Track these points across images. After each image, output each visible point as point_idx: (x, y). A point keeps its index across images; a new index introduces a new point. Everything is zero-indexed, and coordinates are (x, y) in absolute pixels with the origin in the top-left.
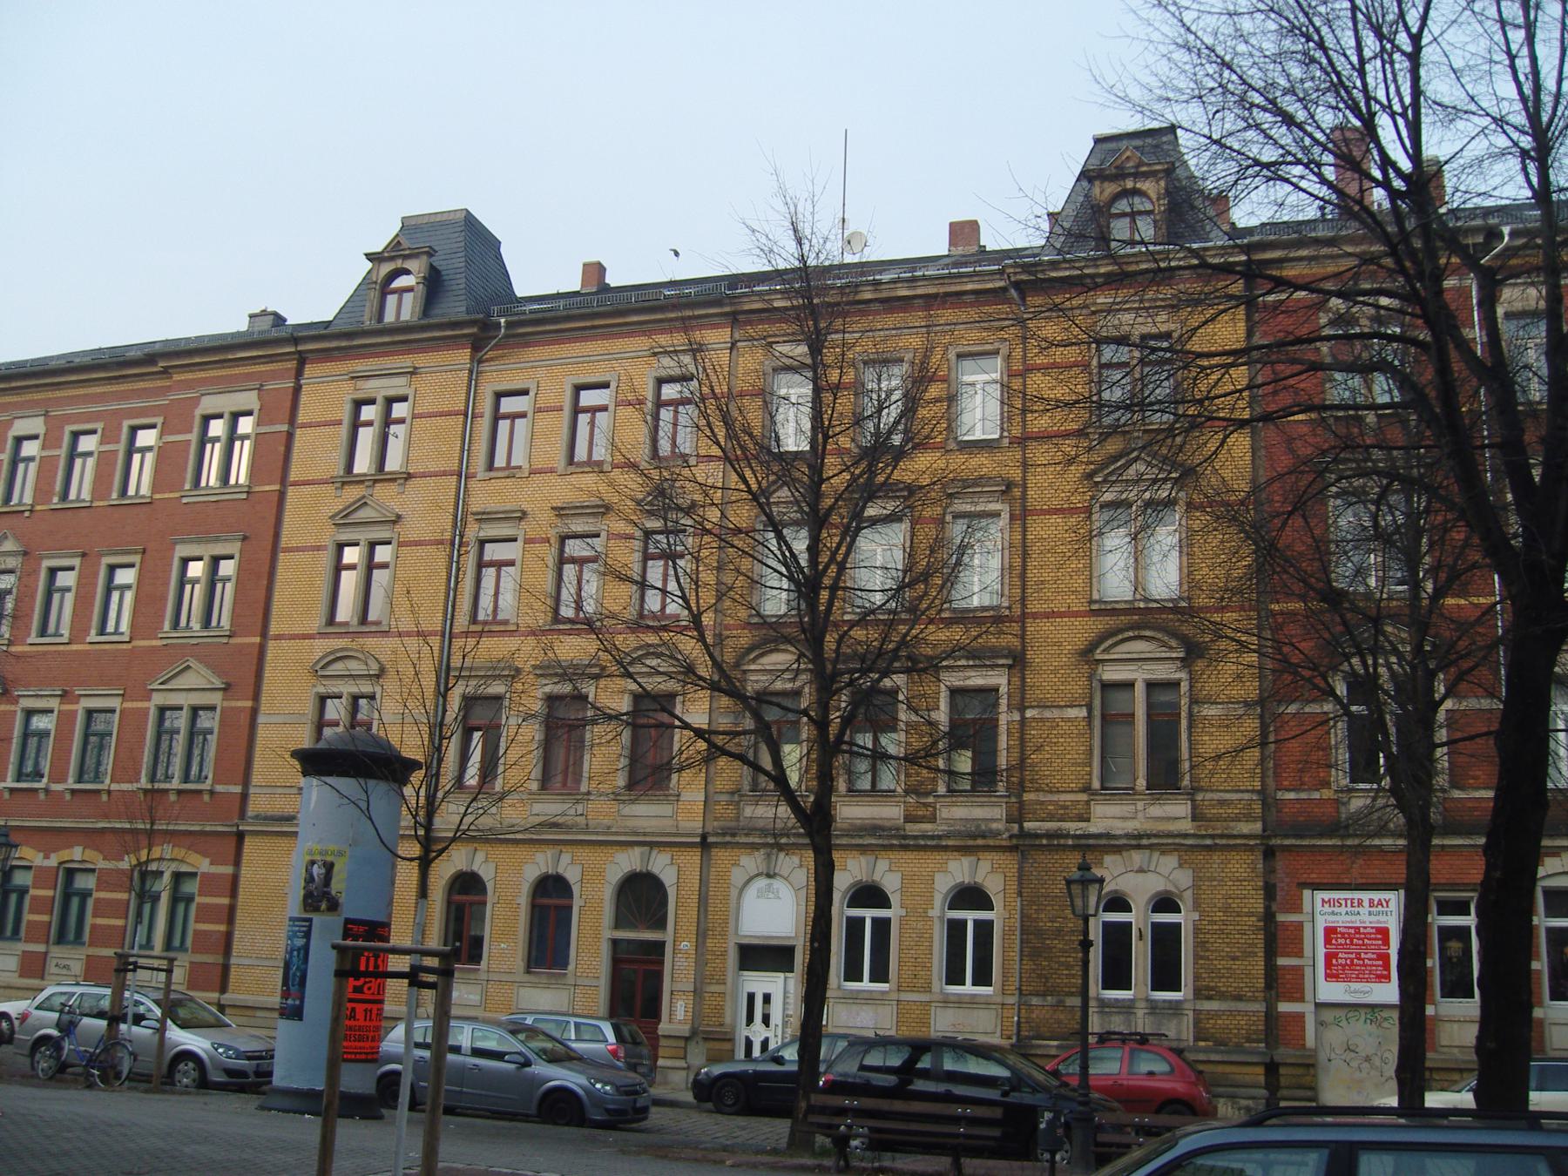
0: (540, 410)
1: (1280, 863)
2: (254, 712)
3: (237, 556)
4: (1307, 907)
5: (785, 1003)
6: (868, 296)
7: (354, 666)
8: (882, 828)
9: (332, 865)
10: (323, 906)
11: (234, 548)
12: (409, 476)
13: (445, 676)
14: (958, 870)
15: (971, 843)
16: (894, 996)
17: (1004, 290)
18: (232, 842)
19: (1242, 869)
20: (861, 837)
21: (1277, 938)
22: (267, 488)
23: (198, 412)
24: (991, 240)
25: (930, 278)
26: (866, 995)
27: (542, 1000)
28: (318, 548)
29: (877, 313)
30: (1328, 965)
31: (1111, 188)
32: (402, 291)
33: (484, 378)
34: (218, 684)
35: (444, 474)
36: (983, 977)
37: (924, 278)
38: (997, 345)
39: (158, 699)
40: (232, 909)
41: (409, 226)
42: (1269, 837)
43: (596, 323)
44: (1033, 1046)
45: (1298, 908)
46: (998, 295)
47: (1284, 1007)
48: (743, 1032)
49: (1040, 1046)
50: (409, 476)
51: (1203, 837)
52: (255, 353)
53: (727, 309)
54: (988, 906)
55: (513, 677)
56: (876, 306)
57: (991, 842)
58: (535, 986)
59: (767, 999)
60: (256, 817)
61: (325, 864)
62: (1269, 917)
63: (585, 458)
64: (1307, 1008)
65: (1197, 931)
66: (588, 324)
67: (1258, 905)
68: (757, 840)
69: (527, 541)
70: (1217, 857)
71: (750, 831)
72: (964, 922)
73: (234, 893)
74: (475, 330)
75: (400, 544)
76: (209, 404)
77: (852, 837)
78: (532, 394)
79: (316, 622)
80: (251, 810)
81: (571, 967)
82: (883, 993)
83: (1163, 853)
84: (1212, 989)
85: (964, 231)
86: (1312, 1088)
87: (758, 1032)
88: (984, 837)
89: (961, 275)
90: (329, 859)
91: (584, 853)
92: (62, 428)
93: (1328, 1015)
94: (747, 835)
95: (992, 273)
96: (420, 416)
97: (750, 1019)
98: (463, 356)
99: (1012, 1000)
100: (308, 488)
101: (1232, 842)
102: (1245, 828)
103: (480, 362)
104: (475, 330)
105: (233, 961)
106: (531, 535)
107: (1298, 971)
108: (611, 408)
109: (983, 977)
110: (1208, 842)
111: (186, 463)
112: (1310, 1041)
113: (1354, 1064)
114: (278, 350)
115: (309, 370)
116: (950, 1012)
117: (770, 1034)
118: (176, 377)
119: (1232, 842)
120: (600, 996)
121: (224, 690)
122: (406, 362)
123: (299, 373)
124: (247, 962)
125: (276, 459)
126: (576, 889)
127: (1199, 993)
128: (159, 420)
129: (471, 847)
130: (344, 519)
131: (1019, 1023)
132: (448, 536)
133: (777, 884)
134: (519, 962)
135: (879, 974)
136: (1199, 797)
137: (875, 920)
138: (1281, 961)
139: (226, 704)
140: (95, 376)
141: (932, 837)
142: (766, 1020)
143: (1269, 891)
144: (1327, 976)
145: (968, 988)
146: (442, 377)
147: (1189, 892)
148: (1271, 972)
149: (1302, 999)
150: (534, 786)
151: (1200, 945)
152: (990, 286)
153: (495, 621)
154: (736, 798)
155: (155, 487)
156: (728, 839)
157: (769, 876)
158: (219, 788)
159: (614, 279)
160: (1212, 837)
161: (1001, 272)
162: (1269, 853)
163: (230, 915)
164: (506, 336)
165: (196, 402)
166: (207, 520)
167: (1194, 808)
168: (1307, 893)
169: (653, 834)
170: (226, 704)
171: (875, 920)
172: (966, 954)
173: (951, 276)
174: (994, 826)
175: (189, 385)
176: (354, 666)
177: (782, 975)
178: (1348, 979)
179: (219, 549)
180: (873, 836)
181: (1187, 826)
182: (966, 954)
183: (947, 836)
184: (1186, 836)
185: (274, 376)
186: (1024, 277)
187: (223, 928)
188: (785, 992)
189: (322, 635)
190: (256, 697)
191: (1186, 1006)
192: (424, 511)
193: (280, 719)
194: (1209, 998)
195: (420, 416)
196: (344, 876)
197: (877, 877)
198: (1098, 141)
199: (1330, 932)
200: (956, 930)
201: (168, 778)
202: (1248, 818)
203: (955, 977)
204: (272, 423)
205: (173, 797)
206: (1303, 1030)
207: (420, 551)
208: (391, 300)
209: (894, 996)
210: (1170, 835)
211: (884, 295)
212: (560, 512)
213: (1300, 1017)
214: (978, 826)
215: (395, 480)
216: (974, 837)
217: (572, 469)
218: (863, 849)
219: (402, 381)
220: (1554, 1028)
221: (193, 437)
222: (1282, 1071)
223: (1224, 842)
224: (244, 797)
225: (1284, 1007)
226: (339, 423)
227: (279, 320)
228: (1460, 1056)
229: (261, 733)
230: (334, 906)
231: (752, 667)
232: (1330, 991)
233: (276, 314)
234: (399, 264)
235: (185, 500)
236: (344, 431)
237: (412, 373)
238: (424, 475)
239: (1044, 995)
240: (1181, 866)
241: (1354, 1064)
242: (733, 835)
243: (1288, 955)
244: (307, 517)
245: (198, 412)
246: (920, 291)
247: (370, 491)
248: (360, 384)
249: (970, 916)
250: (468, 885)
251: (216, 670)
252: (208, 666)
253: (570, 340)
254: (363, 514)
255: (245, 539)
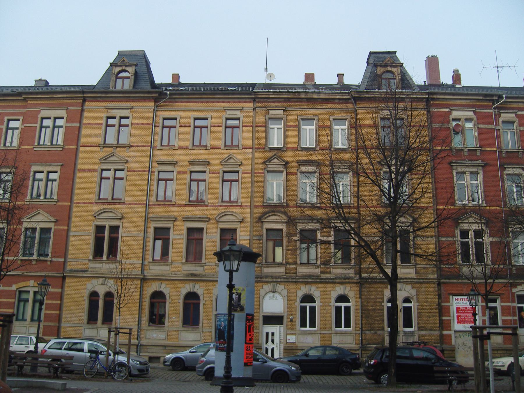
0: (181, 126)
1: (443, 287)
2: (68, 231)
3: (59, 172)
4: (451, 301)
5: (280, 335)
6: (303, 97)
7: (110, 215)
8: (313, 276)
9: (241, 294)
10: (238, 309)
11: (58, 169)
12: (131, 146)
13: (147, 219)
14: (339, 290)
15: (344, 281)
16: (319, 332)
17: (349, 99)
18: (60, 280)
19: (431, 290)
20: (306, 279)
21: (443, 311)
22: (71, 147)
23: (40, 116)
24: (318, 80)
25: (325, 93)
26: (309, 332)
27: (189, 336)
28: (94, 171)
29: (304, 102)
30: (458, 319)
31: (383, 69)
32: (124, 78)
33: (158, 113)
34: (53, 219)
35: (145, 146)
36: (347, 325)
37: (323, 92)
38: (346, 117)
39: (25, 225)
40: (61, 305)
41: (121, 54)
42: (440, 279)
43: (241, 96)
44: (368, 347)
45: (448, 301)
46: (346, 101)
47: (445, 332)
48: (265, 346)
49: (370, 347)
50: (131, 146)
51: (420, 279)
52: (65, 96)
53: (253, 96)
54: (349, 302)
55: (174, 221)
56: (305, 100)
57: (351, 281)
58: (186, 331)
59: (273, 334)
60: (71, 270)
61: (238, 294)
62: (439, 304)
63: (198, 144)
64: (452, 332)
65: (418, 309)
66: (201, 97)
67: (436, 300)
68: (270, 280)
69: (128, 171)
70: (423, 286)
71: (267, 277)
72: (306, 307)
73: (61, 299)
74: (157, 95)
75: (128, 171)
76: (44, 113)
77: (304, 279)
78: (178, 120)
79: (94, 199)
80: (68, 268)
81: (201, 325)
82: (315, 331)
83: (407, 284)
84: (423, 327)
85: (309, 77)
86: (454, 357)
87: (270, 346)
88: (348, 279)
89: (335, 93)
90: (239, 292)
91: (204, 284)
92: (4, 118)
93: (458, 334)
94: (266, 278)
95: (346, 93)
96: (135, 124)
97: (267, 341)
98: (151, 104)
99: (359, 332)
100: (89, 148)
101: (429, 281)
102: (432, 276)
103: (157, 106)
104: (157, 95)
105: (62, 325)
106: (179, 170)
107: (449, 321)
108: (130, 126)
109: (347, 325)
110: (422, 281)
111: (35, 135)
112: (453, 342)
113: (466, 349)
114: (83, 95)
115: (87, 104)
116: (338, 336)
117: (274, 346)
118: (29, 102)
119: (429, 281)
120: (212, 334)
121: (55, 222)
122: (129, 104)
123: (83, 105)
124: (69, 325)
125: (74, 135)
126: (201, 297)
127: (420, 329)
128: (21, 118)
129: (160, 282)
130: (104, 160)
131: (362, 339)
132: (147, 169)
133: (276, 295)
134: (86, 321)
135: (312, 325)
136: (418, 266)
137: (310, 307)
138: (444, 318)
139: (56, 227)
140: (8, 98)
141: (331, 279)
142: (273, 341)
143: (439, 296)
144: (458, 322)
145: (343, 329)
146: (143, 111)
147: (415, 297)
148: (441, 322)
149: (450, 330)
150: (184, 261)
151: (419, 313)
152: (344, 97)
153: (230, 201)
154: (261, 265)
155: (21, 143)
156: (259, 279)
157: (274, 292)
158: (54, 259)
159: (182, 80)
160: (423, 279)
161: (349, 93)
162: (439, 284)
163: (60, 307)
164: (169, 98)
165: (39, 112)
166: (47, 157)
167: (416, 270)
168: (451, 297)
169: (156, 276)
170: (56, 227)
171: (310, 307)
172: (342, 317)
173: (332, 93)
174: (351, 275)
175: (35, 105)
176: (110, 215)
177: (279, 326)
178: (464, 323)
179: (51, 169)
180: (310, 278)
181: (414, 276)
182: (342, 317)
183: (336, 278)
184: (415, 279)
185: (72, 105)
186: (357, 96)
187: (57, 312)
188: (280, 331)
189: (96, 203)
190: (68, 225)
191: (416, 333)
192: (137, 159)
193: (79, 234)
194: (422, 330)
195: (135, 124)
196: (245, 298)
197: (311, 292)
198: (371, 53)
199: (458, 309)
200: (338, 310)
201: (32, 255)
202: (432, 273)
203: (303, 325)
204: (72, 122)
205: (34, 263)
206: (451, 339)
207: (136, 174)
208: (119, 81)
209: (319, 332)
210: (409, 279)
211: (309, 97)
212: (191, 163)
213: (450, 335)
214: (345, 276)
215: (125, 147)
216: (345, 279)
217: (194, 148)
218: (306, 283)
219: (127, 111)
220: (521, 337)
221: (38, 125)
222: (445, 352)
223: (426, 281)
224: (65, 262)
225: (445, 332)
226: (101, 124)
227: (47, 82)
228: (497, 346)
229: (71, 239)
230: (242, 309)
231: (266, 220)
232: (459, 327)
233: (46, 81)
234: (124, 68)
235: (35, 149)
236: (103, 127)
237: (241, 110)
238: (137, 146)
239: (370, 330)
240: (412, 288)
241: (466, 349)
242: (261, 278)
243: (446, 316)
244: (88, 159)
245: (40, 116)
246: (321, 97)
247: (114, 151)
248: (109, 111)
249: (343, 305)
250: (158, 297)
251: (51, 214)
252: (47, 212)
253: (192, 102)
254: (231, 161)
255: (62, 165)
